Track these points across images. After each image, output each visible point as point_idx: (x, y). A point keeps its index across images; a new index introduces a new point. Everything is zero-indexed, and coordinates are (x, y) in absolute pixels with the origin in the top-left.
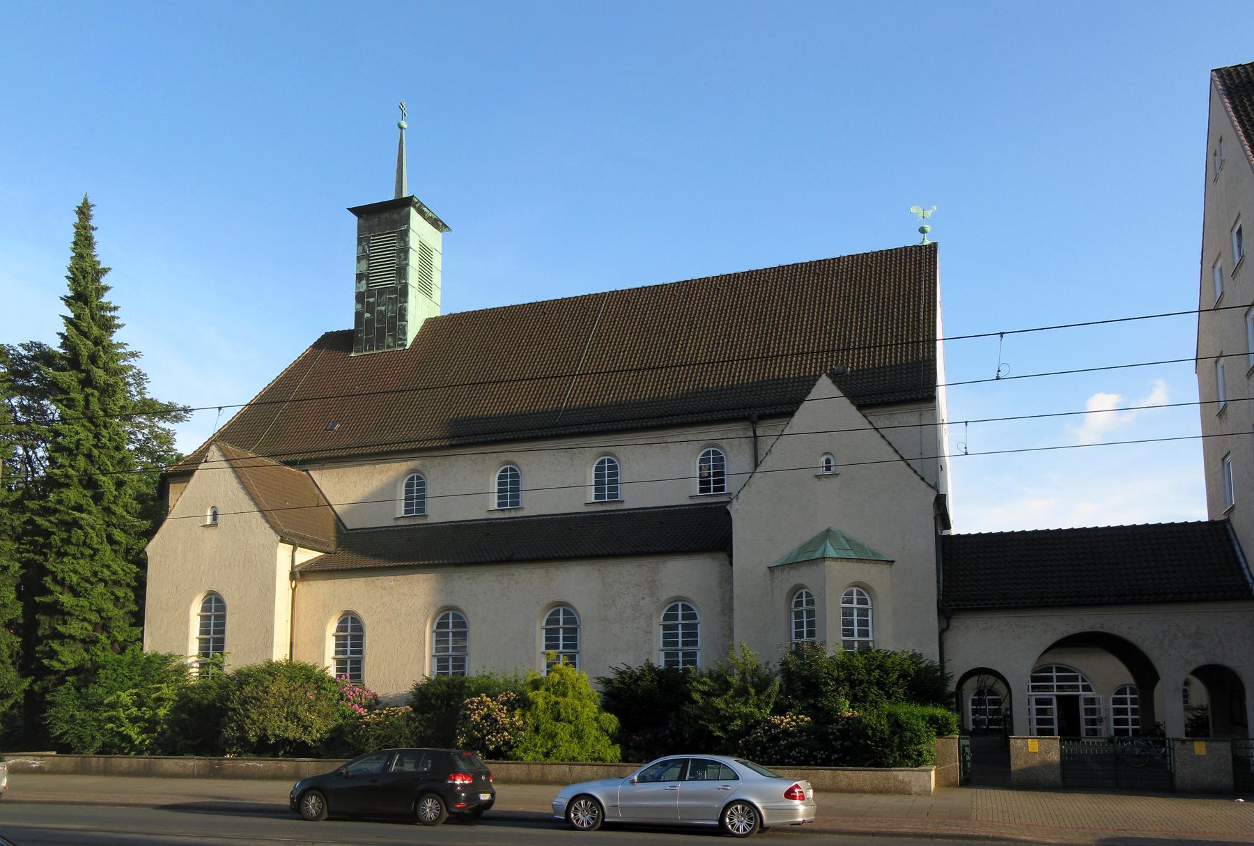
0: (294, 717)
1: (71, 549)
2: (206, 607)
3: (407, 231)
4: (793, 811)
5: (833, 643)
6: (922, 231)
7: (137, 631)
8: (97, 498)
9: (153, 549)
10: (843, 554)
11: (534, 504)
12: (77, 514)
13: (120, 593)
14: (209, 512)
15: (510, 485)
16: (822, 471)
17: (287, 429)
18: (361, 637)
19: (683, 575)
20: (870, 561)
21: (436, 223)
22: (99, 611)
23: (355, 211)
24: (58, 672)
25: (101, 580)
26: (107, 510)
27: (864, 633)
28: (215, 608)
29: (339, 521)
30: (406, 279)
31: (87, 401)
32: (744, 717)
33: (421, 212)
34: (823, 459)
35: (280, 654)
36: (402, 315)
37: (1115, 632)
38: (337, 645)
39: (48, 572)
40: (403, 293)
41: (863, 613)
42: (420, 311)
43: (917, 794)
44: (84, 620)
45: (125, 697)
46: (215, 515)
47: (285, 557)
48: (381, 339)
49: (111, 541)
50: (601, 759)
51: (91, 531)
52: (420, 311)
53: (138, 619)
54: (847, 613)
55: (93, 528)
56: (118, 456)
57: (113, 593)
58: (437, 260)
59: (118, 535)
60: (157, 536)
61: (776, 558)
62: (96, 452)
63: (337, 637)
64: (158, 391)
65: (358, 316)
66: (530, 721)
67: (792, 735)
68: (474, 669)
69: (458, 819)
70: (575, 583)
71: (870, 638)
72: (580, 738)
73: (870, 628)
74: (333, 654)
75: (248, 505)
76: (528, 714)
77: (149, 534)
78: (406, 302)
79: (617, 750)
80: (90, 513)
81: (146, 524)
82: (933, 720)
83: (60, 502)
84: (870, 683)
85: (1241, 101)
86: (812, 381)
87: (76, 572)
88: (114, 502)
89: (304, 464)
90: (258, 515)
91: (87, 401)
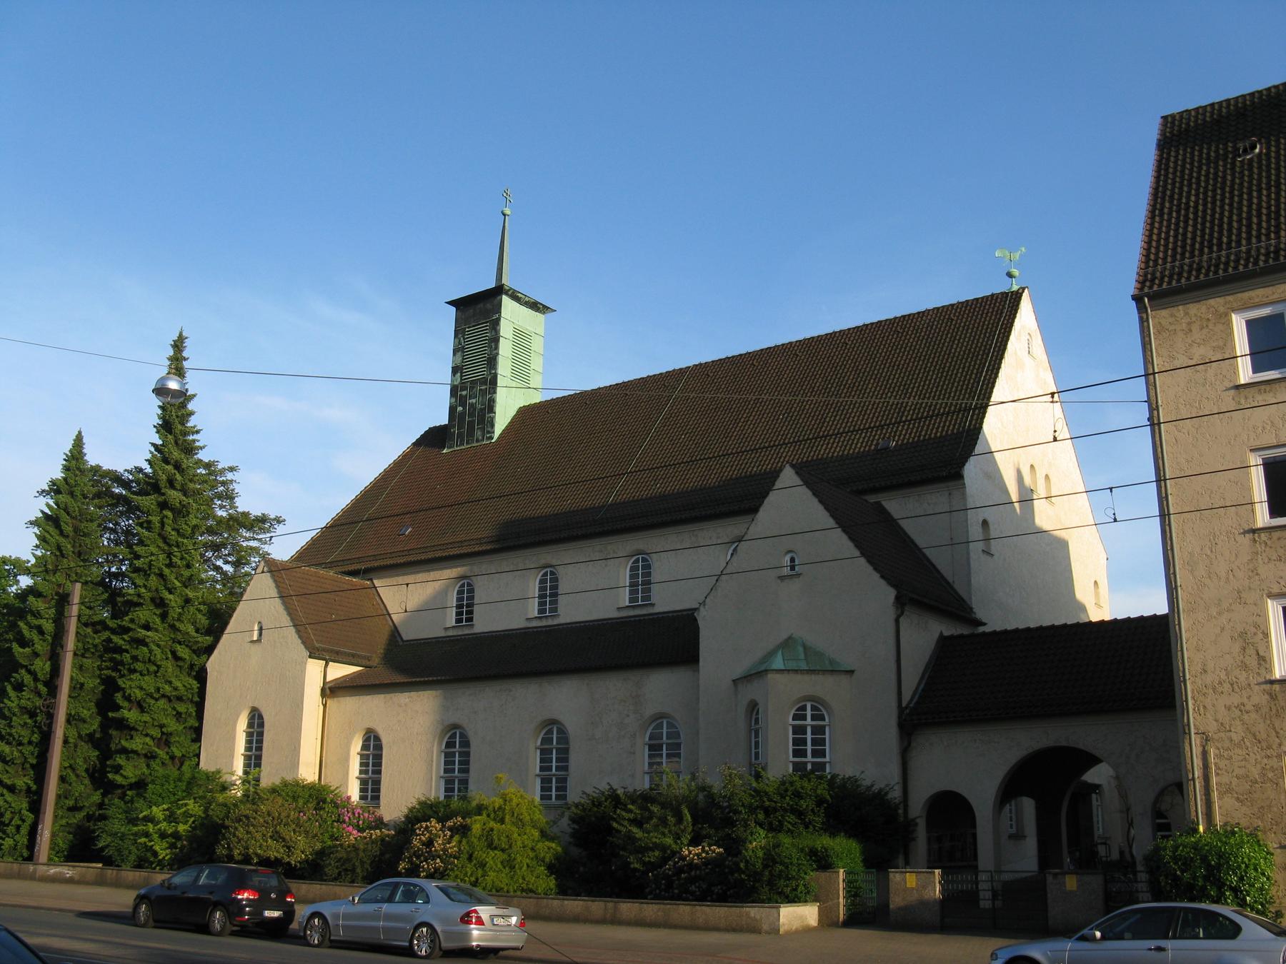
0: (277, 836)
1: (139, 666)
2: (250, 725)
3: (498, 320)
4: (467, 935)
5: (780, 764)
6: (1010, 275)
7: (195, 746)
8: (164, 616)
9: (214, 664)
10: (792, 665)
11: (573, 610)
12: (144, 632)
13: (181, 708)
14: (256, 628)
15: (550, 594)
16: (786, 571)
17: (371, 535)
18: (380, 757)
19: (659, 688)
20: (825, 672)
21: (535, 306)
22: (161, 726)
23: (451, 303)
24: (122, 786)
25: (163, 696)
26: (173, 627)
27: (819, 753)
28: (257, 722)
29: (395, 632)
30: (495, 369)
31: (163, 524)
32: (663, 848)
33: (515, 297)
34: (788, 558)
35: (308, 773)
36: (490, 406)
37: (1081, 746)
38: (361, 764)
39: (119, 689)
40: (493, 382)
41: (819, 730)
42: (508, 403)
43: (767, 932)
44: (147, 735)
45: (157, 812)
46: (261, 629)
47: (315, 673)
48: (471, 432)
49: (176, 657)
50: (531, 891)
51: (154, 647)
52: (508, 403)
53: (197, 734)
54: (799, 730)
55: (158, 646)
56: (186, 573)
57: (174, 709)
58: (537, 345)
59: (183, 652)
60: (216, 652)
61: (739, 671)
62: (166, 571)
63: (362, 756)
64: (248, 503)
65: (452, 410)
66: (464, 846)
67: (697, 867)
68: (478, 794)
69: (244, 931)
70: (566, 699)
71: (827, 759)
72: (512, 867)
73: (827, 748)
74: (357, 773)
75: (286, 620)
76: (464, 841)
77: (209, 650)
78: (495, 392)
79: (552, 882)
80: (157, 630)
81: (209, 639)
82: (813, 853)
83: (132, 621)
84: (785, 810)
85: (1169, 154)
86: (775, 475)
87: (141, 688)
88: (179, 620)
89: (368, 573)
90: (292, 630)
91: (163, 524)
